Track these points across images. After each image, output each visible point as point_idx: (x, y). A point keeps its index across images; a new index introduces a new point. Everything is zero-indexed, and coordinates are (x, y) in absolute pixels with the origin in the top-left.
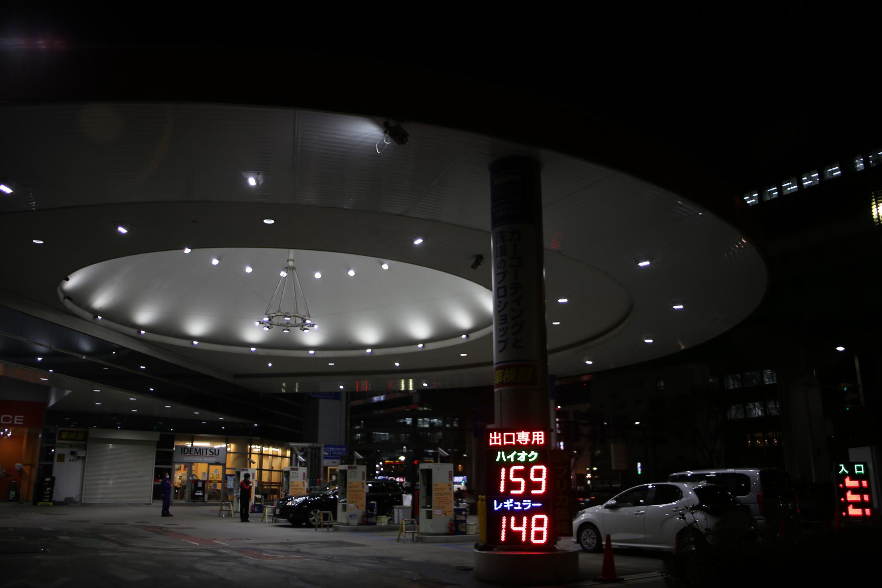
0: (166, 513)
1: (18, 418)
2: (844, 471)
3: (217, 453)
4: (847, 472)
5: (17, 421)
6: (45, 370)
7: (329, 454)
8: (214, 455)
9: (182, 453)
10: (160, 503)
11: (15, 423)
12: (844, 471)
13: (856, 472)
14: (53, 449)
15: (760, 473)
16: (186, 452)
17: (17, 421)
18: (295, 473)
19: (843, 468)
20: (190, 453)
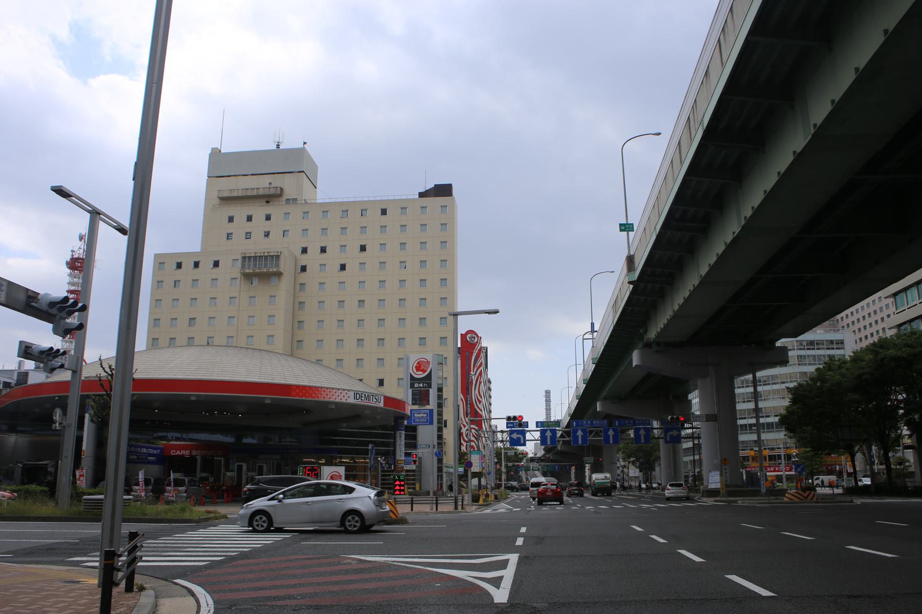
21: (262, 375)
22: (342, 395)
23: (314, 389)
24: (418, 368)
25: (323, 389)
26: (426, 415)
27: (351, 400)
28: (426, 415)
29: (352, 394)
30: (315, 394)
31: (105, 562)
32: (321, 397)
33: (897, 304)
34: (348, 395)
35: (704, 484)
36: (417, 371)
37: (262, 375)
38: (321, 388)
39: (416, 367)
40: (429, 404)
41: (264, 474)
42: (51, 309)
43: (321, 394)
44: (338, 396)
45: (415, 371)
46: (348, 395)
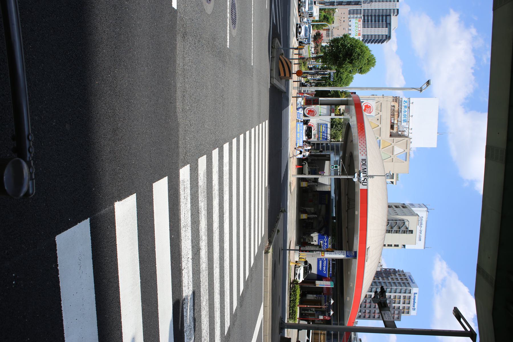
9: (362, 159)
20: (362, 165)
21: (374, 194)
22: (363, 150)
23: (364, 133)
24: (367, 106)
25: (365, 152)
26: (324, 131)
27: (361, 157)
28: (324, 131)
29: (364, 157)
30: (361, 134)
31: (339, 325)
32: (359, 141)
33: (289, 245)
34: (363, 154)
35: (391, 298)
36: (365, 106)
37: (374, 194)
38: (365, 140)
39: (367, 105)
40: (326, 45)
41: (343, 249)
42: (363, 4)
43: (361, 137)
44: (362, 147)
45: (365, 104)
46: (363, 154)
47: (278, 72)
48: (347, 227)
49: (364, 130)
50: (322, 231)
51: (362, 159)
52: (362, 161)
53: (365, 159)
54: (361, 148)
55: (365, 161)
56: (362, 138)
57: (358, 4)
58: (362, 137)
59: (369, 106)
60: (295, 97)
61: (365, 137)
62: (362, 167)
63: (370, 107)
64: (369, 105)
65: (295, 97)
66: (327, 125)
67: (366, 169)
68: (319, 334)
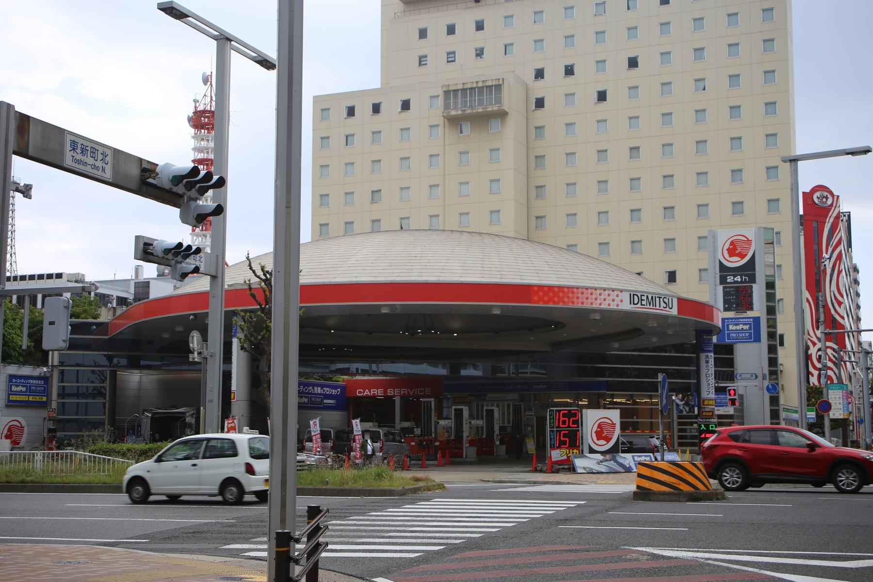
0: (260, 264)
1: (380, 391)
2: (703, 429)
3: (671, 307)
4: (705, 429)
5: (380, 393)
6: (506, 449)
7: (26, 390)
8: (639, 295)
9: (631, 304)
10: (263, 265)
11: (379, 394)
12: (703, 429)
13: (711, 429)
14: (726, 307)
15: (354, 419)
16: (636, 302)
17: (380, 393)
18: (532, 431)
19: (703, 427)
20: (641, 305)
24: (732, 252)
27: (626, 306)
29: (626, 297)
32: (587, 303)
34: (619, 298)
39: (728, 250)
43: (578, 298)
46: (619, 298)
47: (153, 260)
48: (370, 333)
49: (566, 290)
50: (626, 464)
51: (631, 304)
52: (634, 304)
53: (630, 294)
54: (607, 302)
55: (634, 295)
56: (580, 295)
57: (772, 418)
58: (576, 295)
59: (730, 245)
60: (444, 147)
61: (578, 288)
62: (648, 306)
63: (732, 243)
64: (727, 246)
65: (444, 147)
66: (11, 377)
67: (647, 297)
68: (652, 418)
